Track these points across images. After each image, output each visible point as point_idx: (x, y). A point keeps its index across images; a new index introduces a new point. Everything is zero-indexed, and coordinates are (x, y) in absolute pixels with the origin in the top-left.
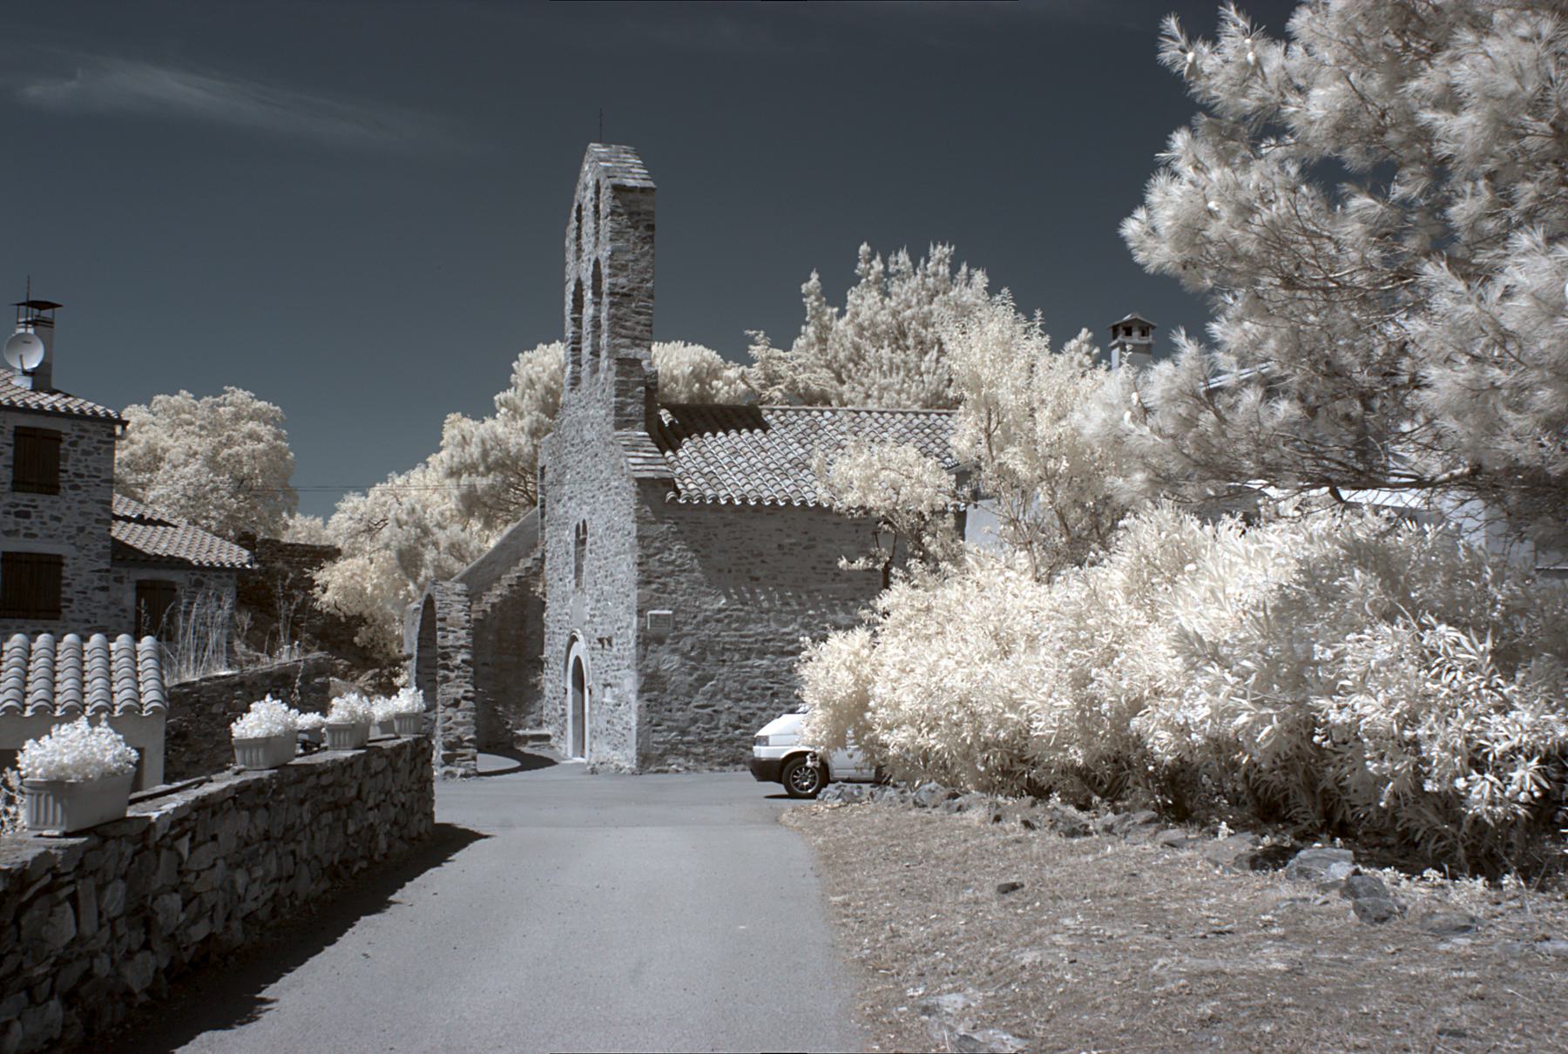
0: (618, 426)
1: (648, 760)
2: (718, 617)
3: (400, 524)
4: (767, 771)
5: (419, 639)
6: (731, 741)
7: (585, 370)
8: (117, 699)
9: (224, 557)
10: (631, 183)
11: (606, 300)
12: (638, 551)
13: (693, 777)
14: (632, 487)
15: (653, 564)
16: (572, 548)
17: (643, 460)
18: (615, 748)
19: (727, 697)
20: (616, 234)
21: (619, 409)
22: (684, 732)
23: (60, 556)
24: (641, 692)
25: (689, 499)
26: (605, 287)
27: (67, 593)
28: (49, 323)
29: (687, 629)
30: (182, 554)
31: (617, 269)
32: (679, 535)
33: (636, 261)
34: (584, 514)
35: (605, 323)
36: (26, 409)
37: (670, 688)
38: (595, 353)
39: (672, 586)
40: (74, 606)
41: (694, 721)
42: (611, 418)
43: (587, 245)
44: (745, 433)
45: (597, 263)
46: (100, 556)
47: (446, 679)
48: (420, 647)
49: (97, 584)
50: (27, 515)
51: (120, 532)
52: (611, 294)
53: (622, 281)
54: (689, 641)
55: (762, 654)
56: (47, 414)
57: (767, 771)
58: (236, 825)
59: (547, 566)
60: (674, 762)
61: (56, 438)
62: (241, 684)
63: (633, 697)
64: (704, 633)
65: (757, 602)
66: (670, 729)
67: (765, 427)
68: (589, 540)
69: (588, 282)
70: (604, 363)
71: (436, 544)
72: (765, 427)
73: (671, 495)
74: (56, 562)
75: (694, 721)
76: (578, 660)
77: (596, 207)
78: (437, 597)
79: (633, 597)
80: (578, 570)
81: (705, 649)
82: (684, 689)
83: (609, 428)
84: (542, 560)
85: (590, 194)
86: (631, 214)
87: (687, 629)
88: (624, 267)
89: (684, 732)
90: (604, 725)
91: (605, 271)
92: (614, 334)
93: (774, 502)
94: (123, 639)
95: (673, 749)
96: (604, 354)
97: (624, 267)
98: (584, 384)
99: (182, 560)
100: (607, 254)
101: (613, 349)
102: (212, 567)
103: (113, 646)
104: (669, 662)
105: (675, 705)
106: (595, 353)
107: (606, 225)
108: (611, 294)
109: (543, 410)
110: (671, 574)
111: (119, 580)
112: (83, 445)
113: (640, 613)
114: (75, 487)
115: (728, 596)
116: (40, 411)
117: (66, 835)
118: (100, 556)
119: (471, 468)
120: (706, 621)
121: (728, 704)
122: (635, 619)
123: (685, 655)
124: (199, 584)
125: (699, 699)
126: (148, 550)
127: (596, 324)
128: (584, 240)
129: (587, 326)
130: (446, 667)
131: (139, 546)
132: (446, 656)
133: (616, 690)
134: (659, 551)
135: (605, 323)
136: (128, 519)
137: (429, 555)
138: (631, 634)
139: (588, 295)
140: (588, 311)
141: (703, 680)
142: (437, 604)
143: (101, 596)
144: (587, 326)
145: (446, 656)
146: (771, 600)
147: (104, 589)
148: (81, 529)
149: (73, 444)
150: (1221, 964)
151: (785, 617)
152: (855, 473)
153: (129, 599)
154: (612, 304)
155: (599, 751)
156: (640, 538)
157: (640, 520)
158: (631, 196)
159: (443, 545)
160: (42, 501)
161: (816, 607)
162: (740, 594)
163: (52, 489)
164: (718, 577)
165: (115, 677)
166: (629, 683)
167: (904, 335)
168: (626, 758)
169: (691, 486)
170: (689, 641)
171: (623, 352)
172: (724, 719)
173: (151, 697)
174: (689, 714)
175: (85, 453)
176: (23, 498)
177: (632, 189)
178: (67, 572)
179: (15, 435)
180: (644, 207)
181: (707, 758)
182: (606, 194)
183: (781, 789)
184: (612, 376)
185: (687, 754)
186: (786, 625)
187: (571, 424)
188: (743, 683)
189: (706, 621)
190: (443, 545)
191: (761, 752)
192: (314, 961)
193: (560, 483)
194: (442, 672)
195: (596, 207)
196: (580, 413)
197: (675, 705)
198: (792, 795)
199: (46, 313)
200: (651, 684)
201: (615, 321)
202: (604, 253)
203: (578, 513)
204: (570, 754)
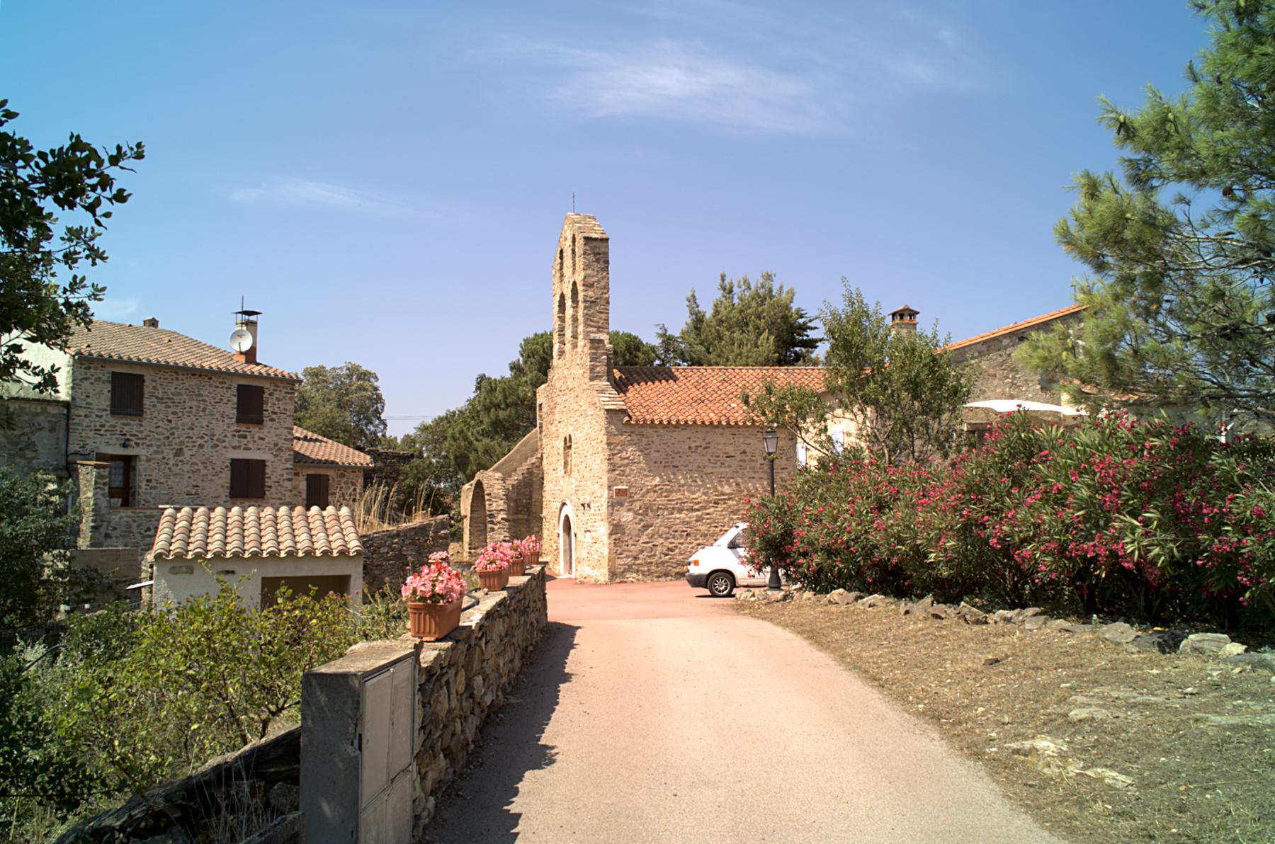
0: (592, 379)
1: (615, 575)
2: (653, 489)
3: (454, 438)
4: (697, 581)
5: (472, 506)
6: (663, 563)
7: (568, 347)
8: (333, 545)
9: (356, 460)
10: (594, 236)
11: (581, 305)
12: (608, 452)
13: (642, 586)
14: (602, 414)
15: (617, 458)
16: (562, 451)
17: (613, 400)
18: (593, 568)
19: (660, 536)
20: (587, 266)
21: (592, 369)
22: (636, 558)
23: (264, 461)
24: (611, 534)
25: (637, 421)
26: (581, 297)
27: (268, 482)
28: (255, 323)
29: (636, 497)
30: (332, 458)
31: (588, 286)
32: (631, 443)
33: (598, 282)
34: (570, 430)
35: (581, 319)
36: (244, 375)
37: (627, 532)
38: (575, 337)
39: (628, 471)
40: (273, 490)
41: (642, 551)
42: (587, 375)
43: (567, 271)
44: (664, 383)
45: (574, 284)
46: (287, 461)
47: (493, 529)
48: (472, 511)
49: (286, 476)
50: (245, 437)
51: (300, 447)
52: (585, 301)
53: (590, 293)
54: (638, 504)
55: (680, 511)
56: (256, 377)
57: (697, 581)
58: (500, 627)
59: (545, 462)
60: (631, 576)
61: (261, 390)
62: (398, 535)
63: (605, 538)
64: (647, 499)
65: (678, 481)
66: (628, 557)
67: (675, 379)
68: (573, 446)
69: (568, 295)
70: (581, 343)
71: (476, 451)
72: (675, 379)
73: (626, 418)
74: (262, 464)
75: (642, 551)
76: (567, 517)
77: (573, 251)
78: (485, 482)
79: (605, 479)
80: (566, 464)
81: (647, 508)
82: (636, 532)
83: (587, 380)
84: (542, 458)
85: (569, 242)
86: (595, 254)
87: (636, 497)
88: (592, 285)
89: (636, 558)
90: (584, 555)
91: (580, 288)
92: (586, 325)
93: (686, 422)
94: (283, 510)
95: (629, 569)
96: (580, 337)
97: (592, 285)
98: (568, 355)
99: (333, 462)
100: (581, 278)
101: (587, 334)
102: (350, 467)
103: (325, 513)
104: (626, 517)
105: (631, 542)
106: (575, 337)
107: (580, 261)
108: (585, 301)
109: (539, 371)
110: (627, 465)
111: (297, 474)
112: (276, 395)
113: (609, 487)
114: (272, 420)
115: (661, 477)
116: (252, 376)
117: (437, 640)
118: (287, 461)
119: (498, 406)
120: (648, 492)
121: (661, 540)
122: (606, 491)
123: (636, 513)
124: (342, 476)
125: (644, 538)
126: (313, 456)
127: (575, 320)
128: (565, 270)
129: (568, 321)
130: (492, 522)
131: (307, 454)
132: (492, 516)
133: (594, 534)
134: (620, 451)
135: (581, 319)
136: (299, 439)
137: (472, 457)
138: (604, 501)
139: (569, 303)
140: (569, 312)
141: (646, 527)
142: (485, 486)
143: (288, 485)
144: (568, 321)
145: (492, 516)
146: (685, 478)
147: (289, 480)
148: (276, 445)
149: (271, 394)
150: (1246, 721)
151: (693, 489)
152: (347, 414)
153: (303, 485)
154: (585, 308)
155: (582, 570)
156: (608, 444)
157: (608, 433)
158: (595, 243)
159: (480, 450)
160: (254, 430)
161: (711, 482)
162: (667, 475)
163: (259, 422)
164: (655, 466)
165: (330, 532)
166: (603, 530)
167: (747, 324)
168: (602, 574)
169: (637, 414)
170: (638, 504)
171: (592, 336)
172: (658, 550)
173: (354, 545)
174: (638, 547)
175: (278, 400)
176: (243, 428)
177: (596, 239)
178: (268, 470)
179: (238, 390)
180: (603, 250)
181: (650, 573)
182: (580, 243)
183: (707, 592)
184: (586, 350)
185: (637, 571)
186: (694, 493)
187: (559, 379)
188: (670, 528)
189: (648, 492)
190: (480, 450)
191: (694, 570)
192: (554, 716)
193: (552, 413)
194: (490, 526)
195: (573, 251)
196: (566, 372)
197: (631, 542)
198: (714, 596)
199: (253, 318)
200: (617, 529)
201: (588, 317)
202: (579, 278)
203: (564, 431)
204: (562, 572)
